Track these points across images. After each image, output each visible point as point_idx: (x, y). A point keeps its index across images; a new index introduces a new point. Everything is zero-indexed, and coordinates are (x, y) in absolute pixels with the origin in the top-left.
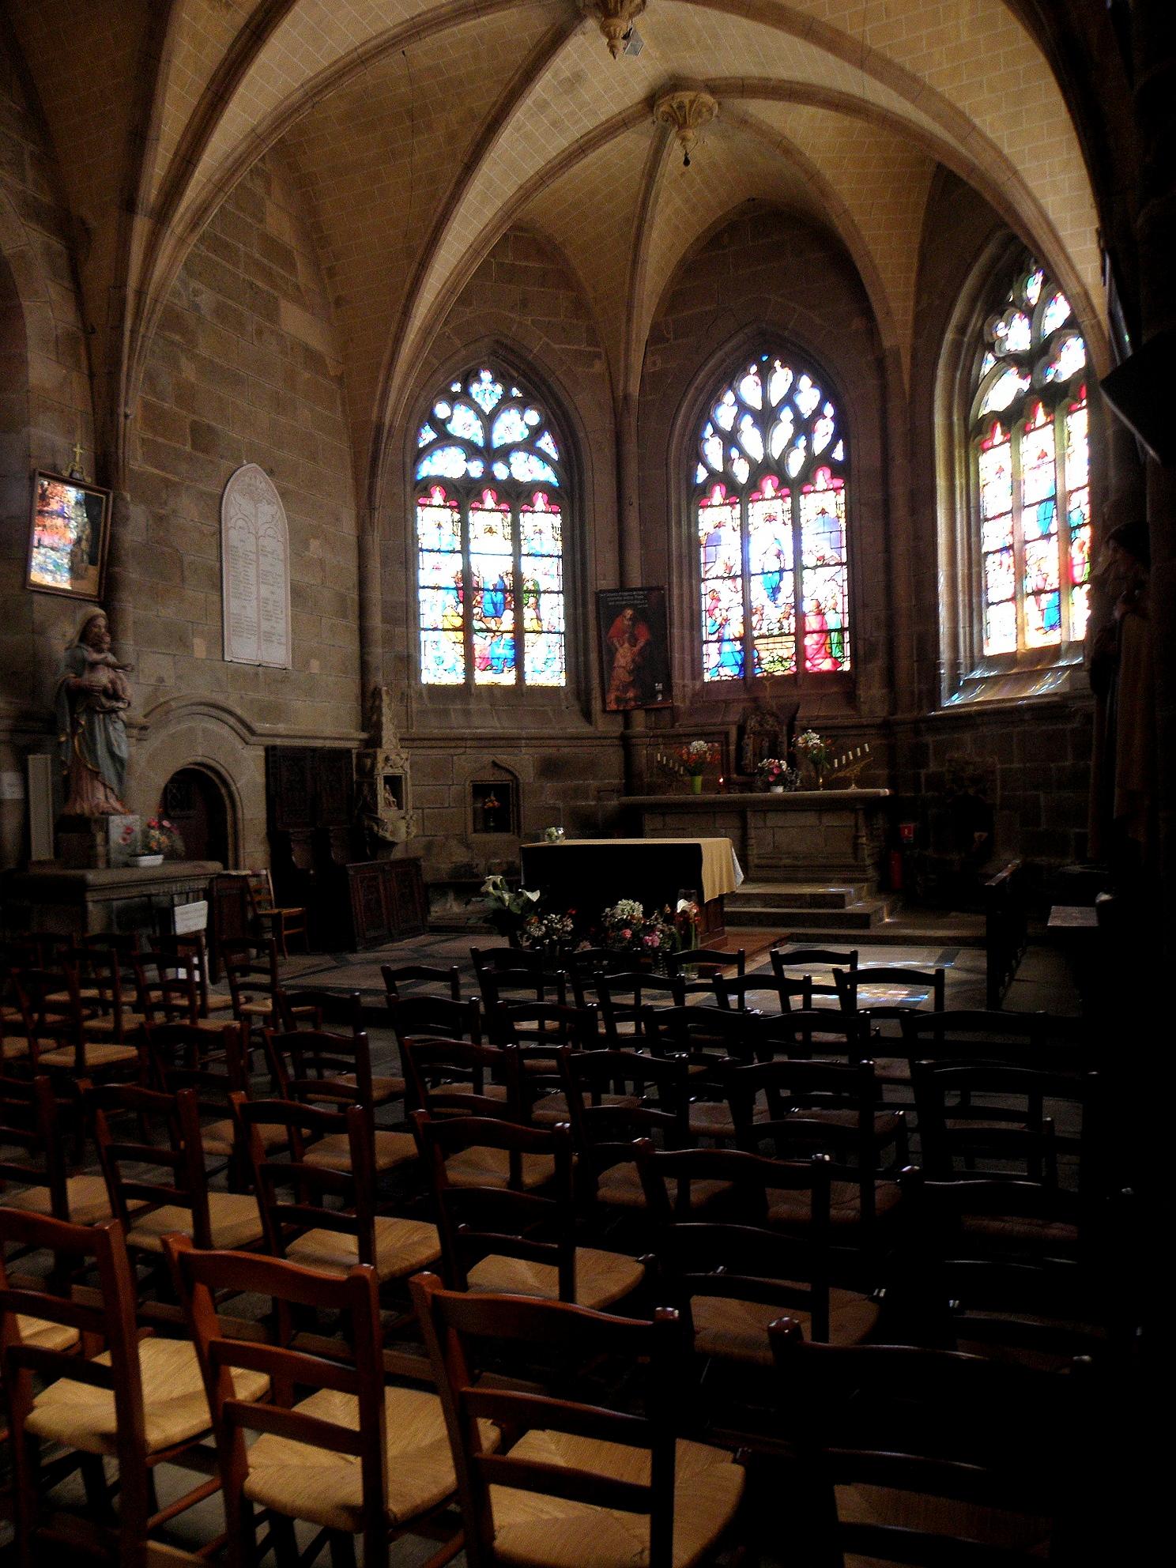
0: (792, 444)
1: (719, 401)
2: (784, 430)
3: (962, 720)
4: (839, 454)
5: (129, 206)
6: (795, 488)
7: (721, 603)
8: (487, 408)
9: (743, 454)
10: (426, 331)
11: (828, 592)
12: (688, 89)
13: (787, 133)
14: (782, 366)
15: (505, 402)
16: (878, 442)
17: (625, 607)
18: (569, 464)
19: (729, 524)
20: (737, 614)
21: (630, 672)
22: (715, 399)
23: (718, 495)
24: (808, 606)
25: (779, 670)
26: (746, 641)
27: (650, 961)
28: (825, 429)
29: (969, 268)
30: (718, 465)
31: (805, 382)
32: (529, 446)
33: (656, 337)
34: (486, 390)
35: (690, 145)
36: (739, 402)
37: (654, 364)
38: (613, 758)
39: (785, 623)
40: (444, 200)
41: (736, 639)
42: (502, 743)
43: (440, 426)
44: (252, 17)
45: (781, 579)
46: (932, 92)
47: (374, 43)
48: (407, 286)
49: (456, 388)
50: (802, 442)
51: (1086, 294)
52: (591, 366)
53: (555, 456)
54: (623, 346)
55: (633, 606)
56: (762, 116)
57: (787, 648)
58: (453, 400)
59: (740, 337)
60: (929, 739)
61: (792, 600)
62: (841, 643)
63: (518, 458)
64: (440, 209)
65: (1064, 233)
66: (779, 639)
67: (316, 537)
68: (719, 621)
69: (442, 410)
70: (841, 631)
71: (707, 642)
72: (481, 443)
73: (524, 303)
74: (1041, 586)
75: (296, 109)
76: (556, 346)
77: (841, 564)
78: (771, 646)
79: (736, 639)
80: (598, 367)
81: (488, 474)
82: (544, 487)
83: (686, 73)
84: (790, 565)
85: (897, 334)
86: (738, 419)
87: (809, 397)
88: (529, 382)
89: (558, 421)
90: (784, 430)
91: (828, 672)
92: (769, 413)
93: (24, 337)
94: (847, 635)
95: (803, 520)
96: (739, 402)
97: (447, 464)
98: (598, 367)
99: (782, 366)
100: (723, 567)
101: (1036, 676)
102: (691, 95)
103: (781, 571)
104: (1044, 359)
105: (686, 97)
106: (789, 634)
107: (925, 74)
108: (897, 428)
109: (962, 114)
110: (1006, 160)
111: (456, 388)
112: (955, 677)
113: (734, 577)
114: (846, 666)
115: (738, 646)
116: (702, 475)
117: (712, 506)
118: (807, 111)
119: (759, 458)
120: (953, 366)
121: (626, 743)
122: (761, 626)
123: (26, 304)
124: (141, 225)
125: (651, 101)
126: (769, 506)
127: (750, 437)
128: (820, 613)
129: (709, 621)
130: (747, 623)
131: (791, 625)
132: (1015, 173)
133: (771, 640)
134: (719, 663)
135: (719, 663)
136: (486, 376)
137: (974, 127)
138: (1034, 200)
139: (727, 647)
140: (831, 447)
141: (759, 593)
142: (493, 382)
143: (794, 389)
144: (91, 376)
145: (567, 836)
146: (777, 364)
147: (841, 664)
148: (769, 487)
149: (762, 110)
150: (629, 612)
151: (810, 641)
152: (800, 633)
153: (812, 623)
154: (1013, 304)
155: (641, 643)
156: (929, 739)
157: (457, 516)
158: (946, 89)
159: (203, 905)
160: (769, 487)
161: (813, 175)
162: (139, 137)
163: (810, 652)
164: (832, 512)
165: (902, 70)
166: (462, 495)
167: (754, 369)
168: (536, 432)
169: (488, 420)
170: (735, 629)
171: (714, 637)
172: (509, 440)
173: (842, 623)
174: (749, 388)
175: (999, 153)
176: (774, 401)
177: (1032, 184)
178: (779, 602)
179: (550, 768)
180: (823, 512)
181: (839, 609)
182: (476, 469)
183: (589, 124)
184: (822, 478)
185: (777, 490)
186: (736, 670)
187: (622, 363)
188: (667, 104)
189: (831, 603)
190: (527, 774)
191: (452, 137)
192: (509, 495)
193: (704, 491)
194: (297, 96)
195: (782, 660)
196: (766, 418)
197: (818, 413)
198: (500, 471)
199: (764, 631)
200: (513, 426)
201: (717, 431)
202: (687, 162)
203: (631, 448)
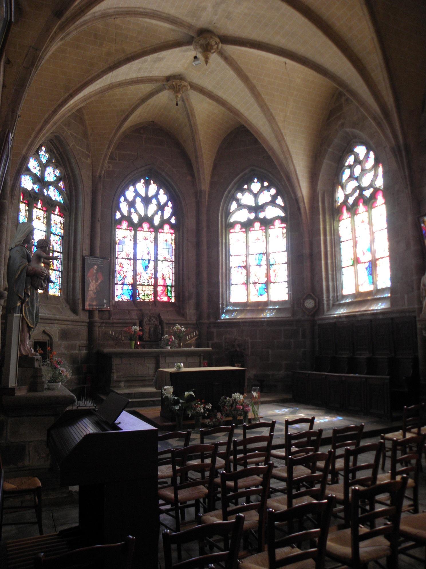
0: (156, 213)
1: (128, 189)
2: (153, 207)
3: (230, 324)
4: (173, 221)
6: (156, 229)
7: (123, 269)
9: (136, 211)
11: (167, 271)
12: (185, 81)
14: (154, 183)
17: (95, 264)
19: (129, 238)
20: (130, 274)
21: (95, 293)
22: (126, 188)
23: (125, 224)
24: (159, 275)
25: (147, 299)
26: (134, 286)
27: (242, 418)
28: (168, 211)
30: (126, 213)
31: (161, 192)
36: (135, 191)
38: (84, 331)
39: (150, 281)
40: (93, 75)
41: (129, 284)
42: (49, 321)
45: (149, 263)
47: (141, 10)
50: (160, 213)
51: (303, 198)
55: (97, 265)
57: (150, 291)
60: (214, 330)
61: (153, 272)
62: (171, 291)
64: (89, 78)
66: (147, 287)
68: (122, 276)
70: (172, 286)
71: (117, 284)
74: (257, 281)
77: (172, 261)
78: (144, 289)
79: (129, 284)
80: (89, 161)
84: (153, 258)
85: (205, 186)
86: (135, 198)
88: (60, 157)
90: (153, 207)
91: (166, 302)
92: (144, 198)
94: (173, 288)
95: (159, 242)
96: (135, 191)
99: (154, 183)
100: (126, 254)
101: (263, 311)
103: (149, 260)
106: (151, 285)
112: (223, 309)
113: (130, 259)
114: (173, 300)
115: (130, 288)
116: (118, 216)
117: (122, 229)
119: (143, 215)
121: (91, 326)
122: (140, 280)
125: (168, 79)
126: (145, 234)
127: (139, 205)
128: (164, 279)
129: (118, 276)
130: (134, 278)
131: (152, 282)
132: (291, 156)
133: (144, 287)
134: (122, 293)
135: (122, 293)
138: (294, 166)
139: (125, 287)
140: (171, 217)
141: (140, 268)
143: (157, 193)
145: (185, 366)
146: (152, 182)
147: (171, 299)
148: (145, 226)
150: (96, 267)
151: (160, 289)
152: (156, 286)
153: (160, 282)
155: (100, 281)
156: (214, 330)
157: (27, 208)
158: (281, 125)
159: (159, 408)
160: (145, 226)
163: (159, 293)
164: (170, 242)
167: (142, 181)
169: (43, 167)
170: (129, 280)
171: (120, 282)
173: (172, 284)
174: (140, 186)
177: (294, 161)
178: (148, 272)
179: (65, 335)
180: (166, 241)
181: (171, 278)
183: (146, 74)
184: (167, 228)
185: (149, 228)
186: (129, 297)
188: (174, 82)
189: (168, 276)
190: (56, 338)
192: (48, 203)
193: (119, 222)
194: (112, 11)
195: (148, 295)
196: (147, 201)
197: (166, 204)
198: (261, 215)
199: (141, 283)
200: (51, 174)
201: (126, 200)
202: (177, 105)
203: (100, 198)
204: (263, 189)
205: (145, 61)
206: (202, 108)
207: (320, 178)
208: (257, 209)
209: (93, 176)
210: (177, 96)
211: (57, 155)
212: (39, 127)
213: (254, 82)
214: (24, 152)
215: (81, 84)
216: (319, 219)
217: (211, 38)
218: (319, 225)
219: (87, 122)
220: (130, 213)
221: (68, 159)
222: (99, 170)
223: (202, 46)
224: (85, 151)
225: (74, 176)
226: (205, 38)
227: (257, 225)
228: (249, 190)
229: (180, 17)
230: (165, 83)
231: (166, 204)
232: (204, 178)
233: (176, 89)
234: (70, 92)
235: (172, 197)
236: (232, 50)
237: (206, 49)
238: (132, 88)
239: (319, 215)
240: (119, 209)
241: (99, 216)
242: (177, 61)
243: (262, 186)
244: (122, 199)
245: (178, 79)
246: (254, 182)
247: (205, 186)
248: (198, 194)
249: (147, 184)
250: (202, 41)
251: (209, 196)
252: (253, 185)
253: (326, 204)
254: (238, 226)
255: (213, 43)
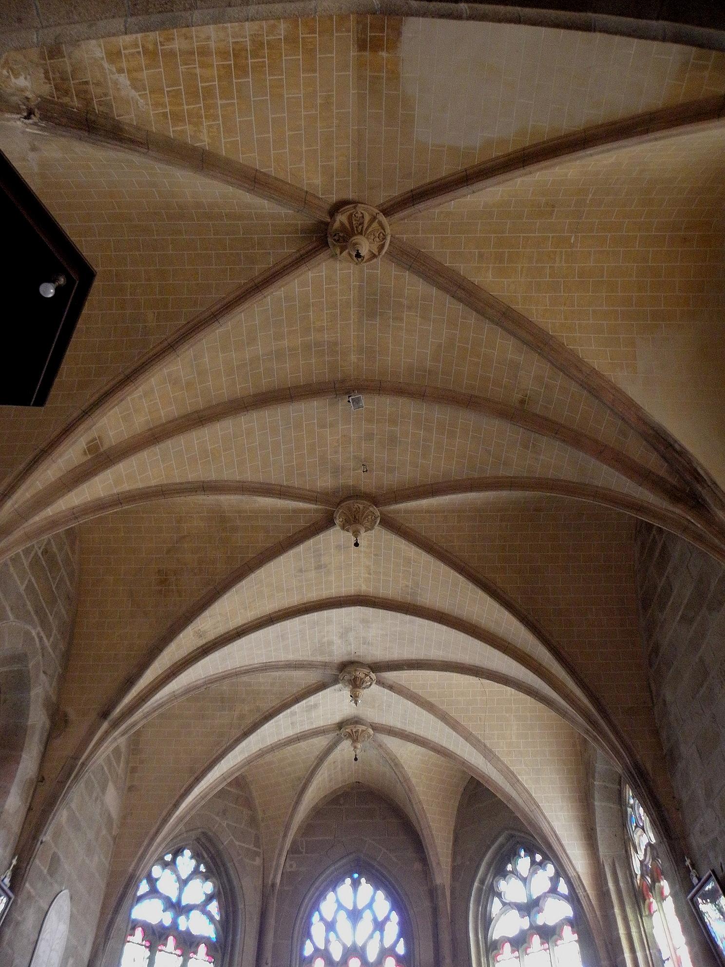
2: (366, 924)
4: (401, 949)
5: (105, 715)
8: (184, 876)
10: (181, 819)
13: (398, 756)
15: (196, 872)
16: (431, 944)
18: (227, 925)
22: (322, 896)
28: (393, 928)
29: (489, 847)
32: (202, 908)
33: (294, 850)
34: (186, 863)
35: (358, 751)
37: (291, 866)
43: (152, 881)
44: (206, 644)
46: (498, 758)
48: (182, 790)
49: (168, 858)
51: (579, 877)
52: (254, 860)
53: (218, 918)
54: (277, 852)
56: (389, 745)
58: (166, 865)
59: (344, 861)
63: (195, 914)
65: (565, 842)
67: (73, 957)
69: (156, 871)
72: (174, 900)
73: (224, 812)
75: (197, 687)
76: (237, 843)
80: (258, 861)
81: (175, 924)
82: (206, 940)
83: (364, 717)
85: (443, 877)
87: (382, 904)
88: (214, 863)
89: (226, 895)
90: (366, 924)
93: (14, 777)
97: (149, 911)
98: (258, 861)
102: (364, 728)
104: (536, 909)
105: (361, 728)
107: (496, 750)
108: (445, 937)
109: (513, 773)
110: (533, 799)
111: (168, 858)
116: (308, 950)
118: (412, 747)
120: (478, 902)
123: (24, 756)
124: (105, 725)
125: (340, 725)
127: (343, 923)
132: (538, 806)
136: (187, 853)
137: (518, 780)
138: (549, 823)
142: (192, 858)
144: (30, 809)
149: (392, 744)
154: (512, 872)
161: (407, 780)
162: (130, 682)
165: (485, 746)
166: (155, 937)
168: (210, 898)
172: (192, 903)
175: (531, 796)
176: (360, 907)
182: (167, 919)
183: (306, 727)
187: (274, 863)
188: (348, 728)
191: (242, 717)
192: (185, 942)
196: (355, 915)
197: (387, 919)
198: (183, 924)
201: (322, 919)
202: (356, 759)
203: (271, 921)
204: (535, 867)
205: (294, 714)
206: (408, 755)
207: (599, 836)
208: (530, 907)
209: (264, 885)
210: (355, 747)
211: (208, 859)
212: (154, 829)
213: (444, 707)
214: (131, 869)
215: (208, 762)
216: (614, 914)
217: (356, 670)
218: (617, 929)
219: (257, 802)
220: (327, 941)
221: (224, 865)
222: (271, 876)
223: (350, 681)
224: (251, 847)
225: (232, 890)
226: (349, 673)
227: (536, 939)
228: (514, 872)
229: (306, 658)
230: (338, 732)
231: (387, 919)
232: (438, 864)
233: (354, 738)
234: (196, 775)
235: (398, 904)
236: (391, 676)
237: (356, 685)
238: (303, 744)
239: (613, 907)
240: (309, 936)
241: (268, 955)
242: (334, 704)
243: (533, 862)
244: (316, 918)
245: (351, 724)
246: (520, 856)
247: (443, 877)
248: (433, 893)
249: (356, 884)
250: (347, 677)
251: (452, 893)
252: (520, 861)
253: (622, 884)
254: (507, 947)
255: (362, 675)
